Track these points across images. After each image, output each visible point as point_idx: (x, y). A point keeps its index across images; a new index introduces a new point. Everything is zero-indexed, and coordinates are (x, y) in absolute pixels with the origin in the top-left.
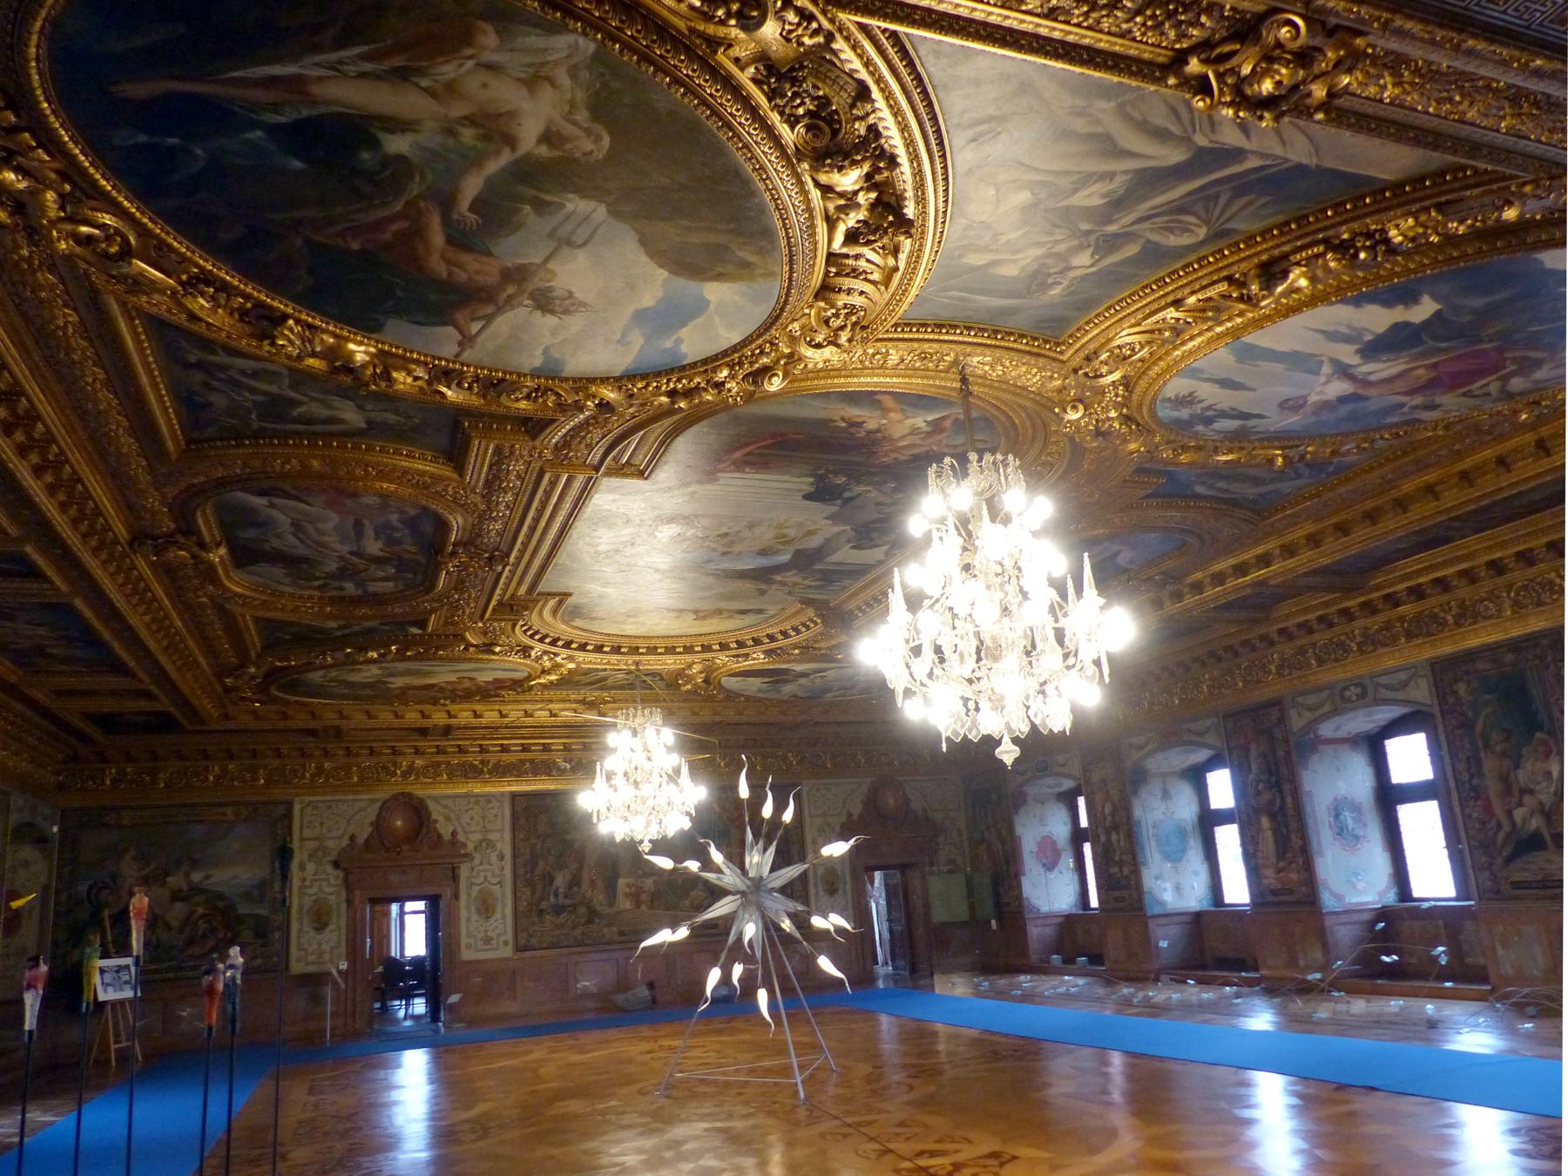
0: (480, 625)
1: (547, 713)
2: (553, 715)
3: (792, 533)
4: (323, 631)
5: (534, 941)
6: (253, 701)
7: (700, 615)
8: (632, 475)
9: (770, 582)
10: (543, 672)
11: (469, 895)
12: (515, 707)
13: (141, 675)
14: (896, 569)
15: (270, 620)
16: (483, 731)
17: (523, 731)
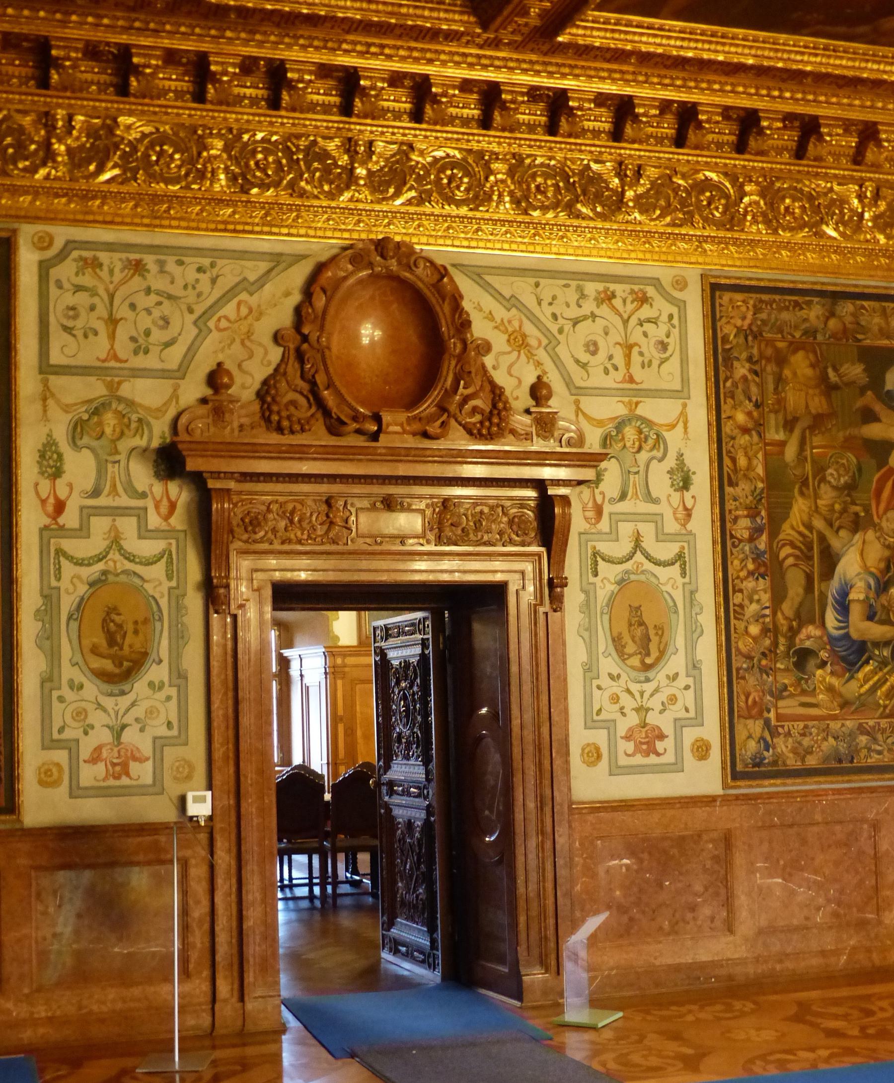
5: (782, 746)
11: (588, 592)
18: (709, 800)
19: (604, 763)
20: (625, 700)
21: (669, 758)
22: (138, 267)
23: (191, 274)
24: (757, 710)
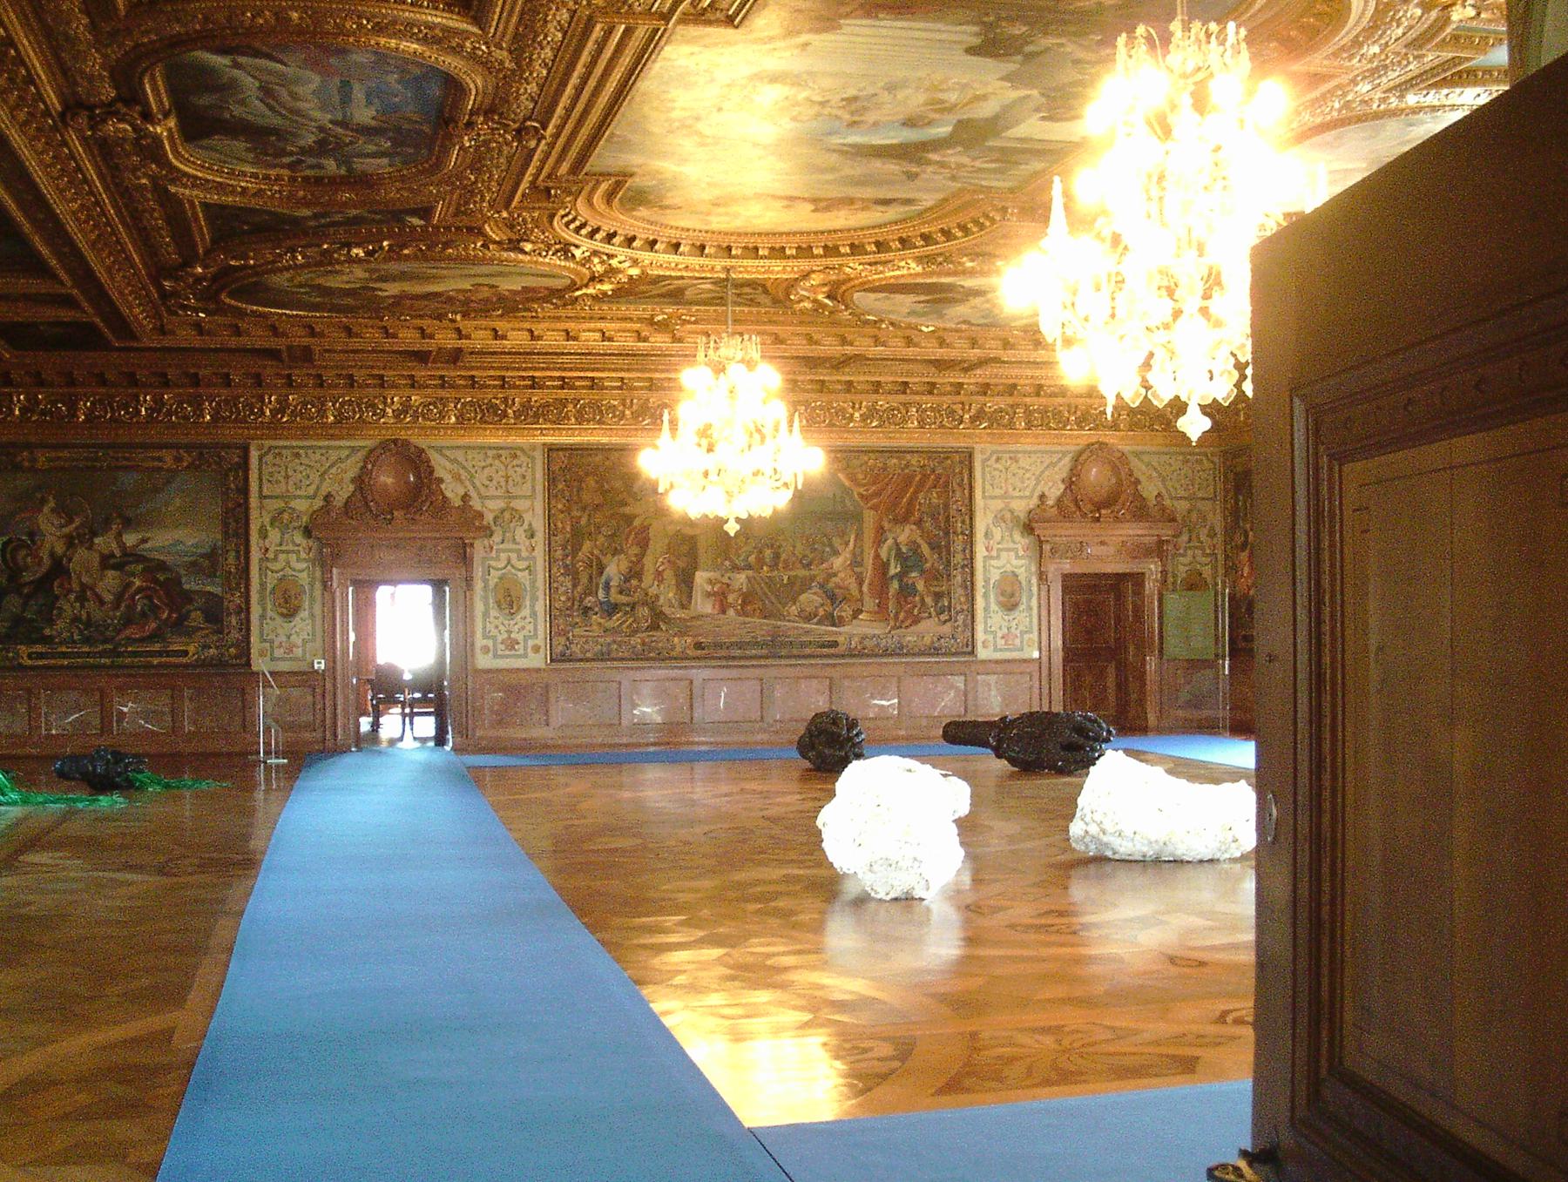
0: (505, 214)
1: (598, 335)
2: (604, 338)
3: (953, 97)
4: (296, 222)
5: (575, 649)
6: (196, 311)
7: (821, 204)
8: (717, 22)
9: (921, 162)
10: (593, 279)
11: (486, 582)
12: (553, 326)
13: (62, 274)
14: (1057, 179)
15: (223, 207)
16: (508, 358)
17: (565, 359)
18: (538, 670)
19: (491, 654)
20: (501, 627)
21: (522, 652)
22: (297, 455)
23: (318, 456)
24: (564, 633)
